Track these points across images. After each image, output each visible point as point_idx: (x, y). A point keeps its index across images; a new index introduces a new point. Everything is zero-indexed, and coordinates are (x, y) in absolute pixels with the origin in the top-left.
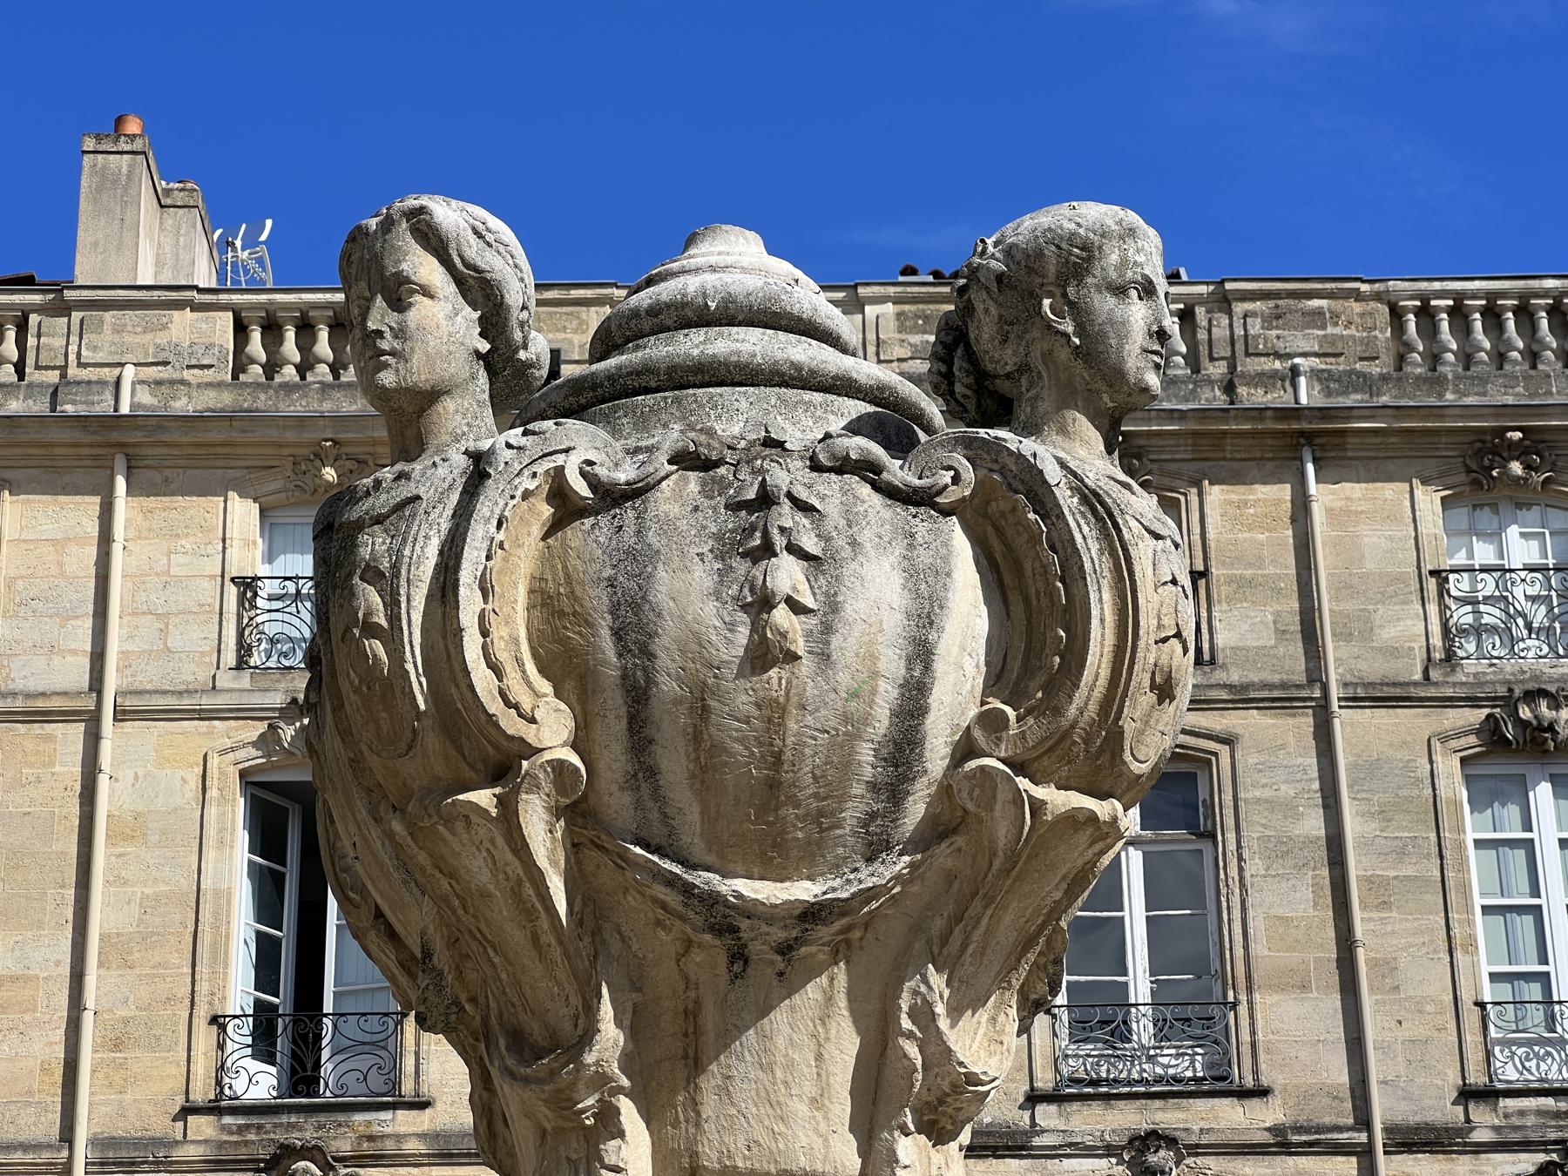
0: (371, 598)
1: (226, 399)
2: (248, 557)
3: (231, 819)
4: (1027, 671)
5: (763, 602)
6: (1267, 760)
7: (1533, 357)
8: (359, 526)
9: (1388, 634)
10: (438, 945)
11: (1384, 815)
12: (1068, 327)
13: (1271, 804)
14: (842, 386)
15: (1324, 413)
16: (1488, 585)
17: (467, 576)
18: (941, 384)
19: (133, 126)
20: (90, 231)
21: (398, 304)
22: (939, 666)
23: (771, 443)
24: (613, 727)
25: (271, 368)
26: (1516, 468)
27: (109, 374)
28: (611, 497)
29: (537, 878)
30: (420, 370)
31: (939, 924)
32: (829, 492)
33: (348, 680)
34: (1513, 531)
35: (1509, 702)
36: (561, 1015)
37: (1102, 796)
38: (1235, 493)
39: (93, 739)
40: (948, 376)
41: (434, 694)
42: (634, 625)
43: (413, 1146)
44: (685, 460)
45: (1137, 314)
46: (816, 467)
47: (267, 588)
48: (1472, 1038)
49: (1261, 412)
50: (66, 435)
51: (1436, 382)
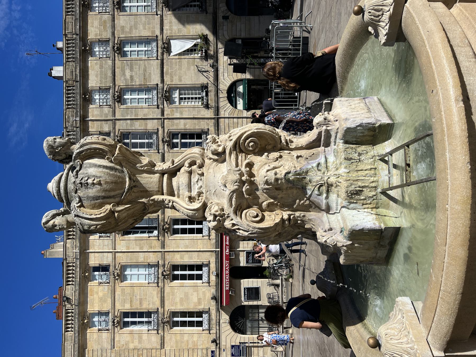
0: (92, 228)
1: (77, 240)
4: (102, 154)
5: (93, 184)
6: (121, 126)
7: (74, 93)
8: (84, 229)
9: (107, 112)
10: (133, 219)
11: (128, 114)
12: (60, 148)
14: (68, 174)
15: (80, 117)
16: (101, 101)
17: (90, 217)
18: (68, 163)
19: (43, 252)
20: (56, 256)
21: (56, 226)
22: (101, 164)
23: (74, 183)
24: (108, 200)
25: (74, 235)
27: (74, 253)
28: (80, 201)
30: (64, 223)
31: (131, 165)
32: (80, 176)
33: (102, 230)
35: (115, 100)
36: (141, 205)
37: (117, 147)
38: (90, 128)
39: (118, 252)
40: (66, 162)
41: (104, 220)
43: (163, 216)
44: (76, 192)
45: (58, 140)
46: (77, 177)
48: (152, 107)
50: (82, 258)
51: (77, 104)
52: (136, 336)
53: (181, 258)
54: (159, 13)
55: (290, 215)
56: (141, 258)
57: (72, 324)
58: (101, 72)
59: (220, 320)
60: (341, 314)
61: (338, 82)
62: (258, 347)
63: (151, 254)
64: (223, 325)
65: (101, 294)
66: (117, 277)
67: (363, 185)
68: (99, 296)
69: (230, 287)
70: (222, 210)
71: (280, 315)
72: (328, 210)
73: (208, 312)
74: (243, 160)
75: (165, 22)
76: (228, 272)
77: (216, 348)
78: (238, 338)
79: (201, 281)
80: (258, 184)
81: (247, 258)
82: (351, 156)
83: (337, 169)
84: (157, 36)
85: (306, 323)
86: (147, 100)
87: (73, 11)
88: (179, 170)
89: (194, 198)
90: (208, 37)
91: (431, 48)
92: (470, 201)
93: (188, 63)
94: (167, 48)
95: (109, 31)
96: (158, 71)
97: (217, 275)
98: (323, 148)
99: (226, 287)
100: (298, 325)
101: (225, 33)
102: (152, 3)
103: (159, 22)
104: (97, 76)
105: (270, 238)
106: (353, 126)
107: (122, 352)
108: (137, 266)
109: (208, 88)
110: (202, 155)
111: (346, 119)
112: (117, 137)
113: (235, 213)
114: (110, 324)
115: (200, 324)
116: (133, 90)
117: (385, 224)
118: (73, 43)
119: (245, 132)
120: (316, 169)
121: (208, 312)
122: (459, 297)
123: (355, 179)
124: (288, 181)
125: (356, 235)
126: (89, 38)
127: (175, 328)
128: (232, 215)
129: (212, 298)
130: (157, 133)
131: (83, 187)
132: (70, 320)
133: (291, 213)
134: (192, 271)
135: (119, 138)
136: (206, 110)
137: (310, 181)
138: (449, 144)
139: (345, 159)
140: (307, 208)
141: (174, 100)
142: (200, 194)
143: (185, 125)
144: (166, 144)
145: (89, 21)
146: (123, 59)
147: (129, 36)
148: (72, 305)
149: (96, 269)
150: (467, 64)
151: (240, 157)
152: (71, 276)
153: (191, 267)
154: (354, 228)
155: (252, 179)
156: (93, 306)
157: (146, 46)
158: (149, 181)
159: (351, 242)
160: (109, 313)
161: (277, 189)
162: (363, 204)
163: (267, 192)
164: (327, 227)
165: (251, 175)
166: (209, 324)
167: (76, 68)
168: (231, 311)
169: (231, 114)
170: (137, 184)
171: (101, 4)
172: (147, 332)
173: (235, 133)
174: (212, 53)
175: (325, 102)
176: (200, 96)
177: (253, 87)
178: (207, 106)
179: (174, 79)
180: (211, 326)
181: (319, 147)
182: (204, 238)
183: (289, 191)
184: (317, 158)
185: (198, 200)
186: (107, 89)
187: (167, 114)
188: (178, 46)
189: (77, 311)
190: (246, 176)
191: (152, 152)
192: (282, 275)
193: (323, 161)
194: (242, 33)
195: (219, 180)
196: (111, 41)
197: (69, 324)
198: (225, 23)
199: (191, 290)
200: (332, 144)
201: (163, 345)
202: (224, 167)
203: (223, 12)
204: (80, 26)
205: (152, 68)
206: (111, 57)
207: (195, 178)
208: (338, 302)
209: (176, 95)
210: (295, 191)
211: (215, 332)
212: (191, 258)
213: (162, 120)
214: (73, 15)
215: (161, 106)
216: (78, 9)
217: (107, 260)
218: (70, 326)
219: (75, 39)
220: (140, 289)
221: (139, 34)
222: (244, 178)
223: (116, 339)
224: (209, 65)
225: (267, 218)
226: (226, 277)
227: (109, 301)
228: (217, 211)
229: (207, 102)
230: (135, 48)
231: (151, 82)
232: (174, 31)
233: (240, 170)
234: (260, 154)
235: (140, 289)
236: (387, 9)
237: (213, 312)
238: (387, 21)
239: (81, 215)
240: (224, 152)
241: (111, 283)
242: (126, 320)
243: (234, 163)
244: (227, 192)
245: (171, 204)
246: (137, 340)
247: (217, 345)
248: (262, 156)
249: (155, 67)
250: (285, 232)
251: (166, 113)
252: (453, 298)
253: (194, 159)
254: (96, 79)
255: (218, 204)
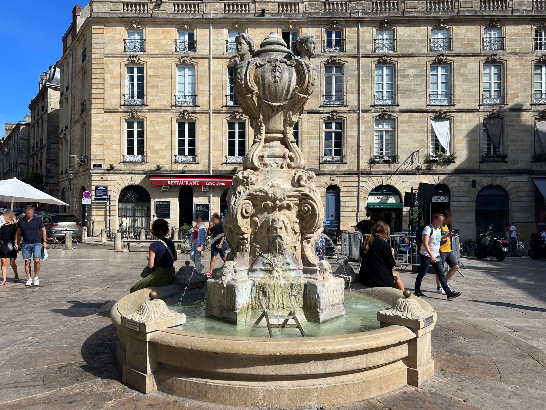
0: (239, 76)
2: (227, 37)
3: (226, 71)
5: (275, 77)
6: (351, 64)
7: (390, 9)
8: (237, 68)
9: (368, 48)
11: (365, 72)
13: (351, 70)
14: (284, 52)
15: (362, 18)
16: (381, 41)
17: (248, 74)
21: (241, 45)
25: (229, 11)
26: (386, 25)
29: (154, 372)
30: (243, 52)
32: (282, 65)
33: (237, 84)
34: (385, 34)
35: (382, 57)
36: (257, 115)
42: (263, 79)
44: (268, 62)
47: (229, 41)
48: (373, 99)
49: (354, 18)
51: (377, 13)
52: (118, 82)
53: (203, 132)
54: (482, 107)
55: (247, 239)
56: (203, 87)
57: (131, 11)
58: (414, 41)
59: (134, 174)
60: (160, 286)
61: (367, 289)
62: (106, 215)
63: (207, 98)
64: (129, 177)
65: (164, 42)
66: (182, 60)
67: (271, 298)
68: (162, 40)
69: (171, 186)
70: (252, 184)
71: (161, 232)
72: (251, 270)
73: (143, 161)
74: (293, 202)
75: (471, 115)
76: (187, 183)
77: (104, 170)
78: (115, 194)
79: (177, 154)
80: (273, 214)
81: (202, 204)
82: (294, 289)
83: (284, 278)
84: (454, 105)
85: (153, 255)
86: (381, 93)
87: (485, 8)
88: (287, 147)
89: (262, 160)
90: (452, 164)
91: (365, 338)
92: (254, 353)
93: (422, 141)
94: (440, 117)
95: (462, 49)
96: (413, 107)
97: (183, 172)
98: (302, 268)
99: (171, 181)
100: (152, 247)
101: (456, 184)
102: (494, 99)
103: (470, 108)
104: (409, 36)
105: (229, 223)
106: (318, 291)
107: (101, 66)
108: (194, 85)
109: (393, 163)
110: (298, 167)
111: (324, 286)
112: (339, 60)
113: (249, 195)
114: (132, 53)
115: (130, 152)
116: (392, 77)
117: (239, 313)
118: (448, 9)
119: (316, 204)
120: (285, 261)
121: (143, 161)
122: (190, 347)
123: (276, 291)
124: (275, 238)
125: (231, 290)
126: (454, 27)
127: (126, 124)
128: (247, 192)
129: (158, 166)
130: (342, 105)
131: (272, 68)
132: (136, 7)
133: (249, 240)
134: (188, 144)
135: (337, 61)
136: (367, 161)
137: (275, 256)
138: (294, 343)
139: (292, 284)
140: (253, 253)
141: (379, 124)
142: (266, 165)
143: (351, 137)
144: (330, 116)
145: (473, 27)
146: (429, 66)
147: (456, 74)
148: (152, 10)
149: (191, 37)
150: (353, 363)
151: (295, 199)
152: (184, 8)
153: (192, 143)
154: (236, 288)
155: (277, 209)
156: (151, 34)
157: (443, 93)
158: (278, 122)
159: (225, 286)
160: (143, 51)
161: (269, 229)
162: (255, 297)
163: (266, 221)
164: (237, 269)
165: (281, 208)
166: (131, 163)
167: (419, 12)
168: (144, 186)
169: (363, 189)
170: (275, 112)
171: (493, 41)
172: (122, 93)
173: (316, 196)
174: (434, 168)
175: (350, 277)
176: (384, 154)
177: (394, 214)
178: (372, 162)
179: (404, 125)
180: (128, 164)
181: (304, 265)
182: (224, 158)
183: (267, 239)
184: (294, 263)
185: (261, 164)
186: (394, 48)
187: (363, 116)
188: (442, 129)
189: (146, 16)
190: (280, 204)
191: (322, 99)
192: (184, 242)
193: (291, 267)
194: (456, 203)
195: (275, 181)
196: (449, 52)
197: (131, 7)
198: (467, 184)
199: (167, 142)
200: (305, 275)
201: (109, 111)
202: (287, 186)
203: (481, 181)
204: (467, 16)
205: (417, 100)
206: (430, 53)
207: (279, 161)
208: (171, 284)
209: (386, 126)
210: (267, 244)
211: (122, 168)
212: (202, 143)
213: (358, 111)
214: (481, 8)
215: (373, 109)
216: (488, 13)
217: (201, 48)
218: (129, 8)
219: (452, 11)
220: (169, 86)
221: (458, 85)
222: (278, 202)
223: (115, 60)
224: (420, 165)
225: (245, 220)
226: (181, 181)
227: (156, 52)
228: (251, 179)
229: (377, 162)
230: (441, 79)
231: (401, 98)
232: (459, 124)
233: (285, 199)
234: (299, 216)
235: (169, 86)
236: (405, 314)
237: (143, 167)
238: (396, 314)
239: (249, 67)
240: (301, 186)
241: (176, 53)
242: (136, 70)
243: (290, 194)
244: (266, 188)
245: (258, 140)
246: (113, 83)
247: (107, 170)
248: (297, 217)
249: (418, 103)
250: (233, 236)
251: (365, 115)
252: (189, 344)
253: (295, 160)
254: (406, 35)
255: (257, 180)
